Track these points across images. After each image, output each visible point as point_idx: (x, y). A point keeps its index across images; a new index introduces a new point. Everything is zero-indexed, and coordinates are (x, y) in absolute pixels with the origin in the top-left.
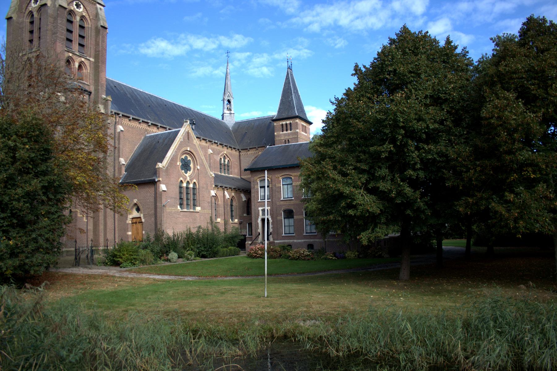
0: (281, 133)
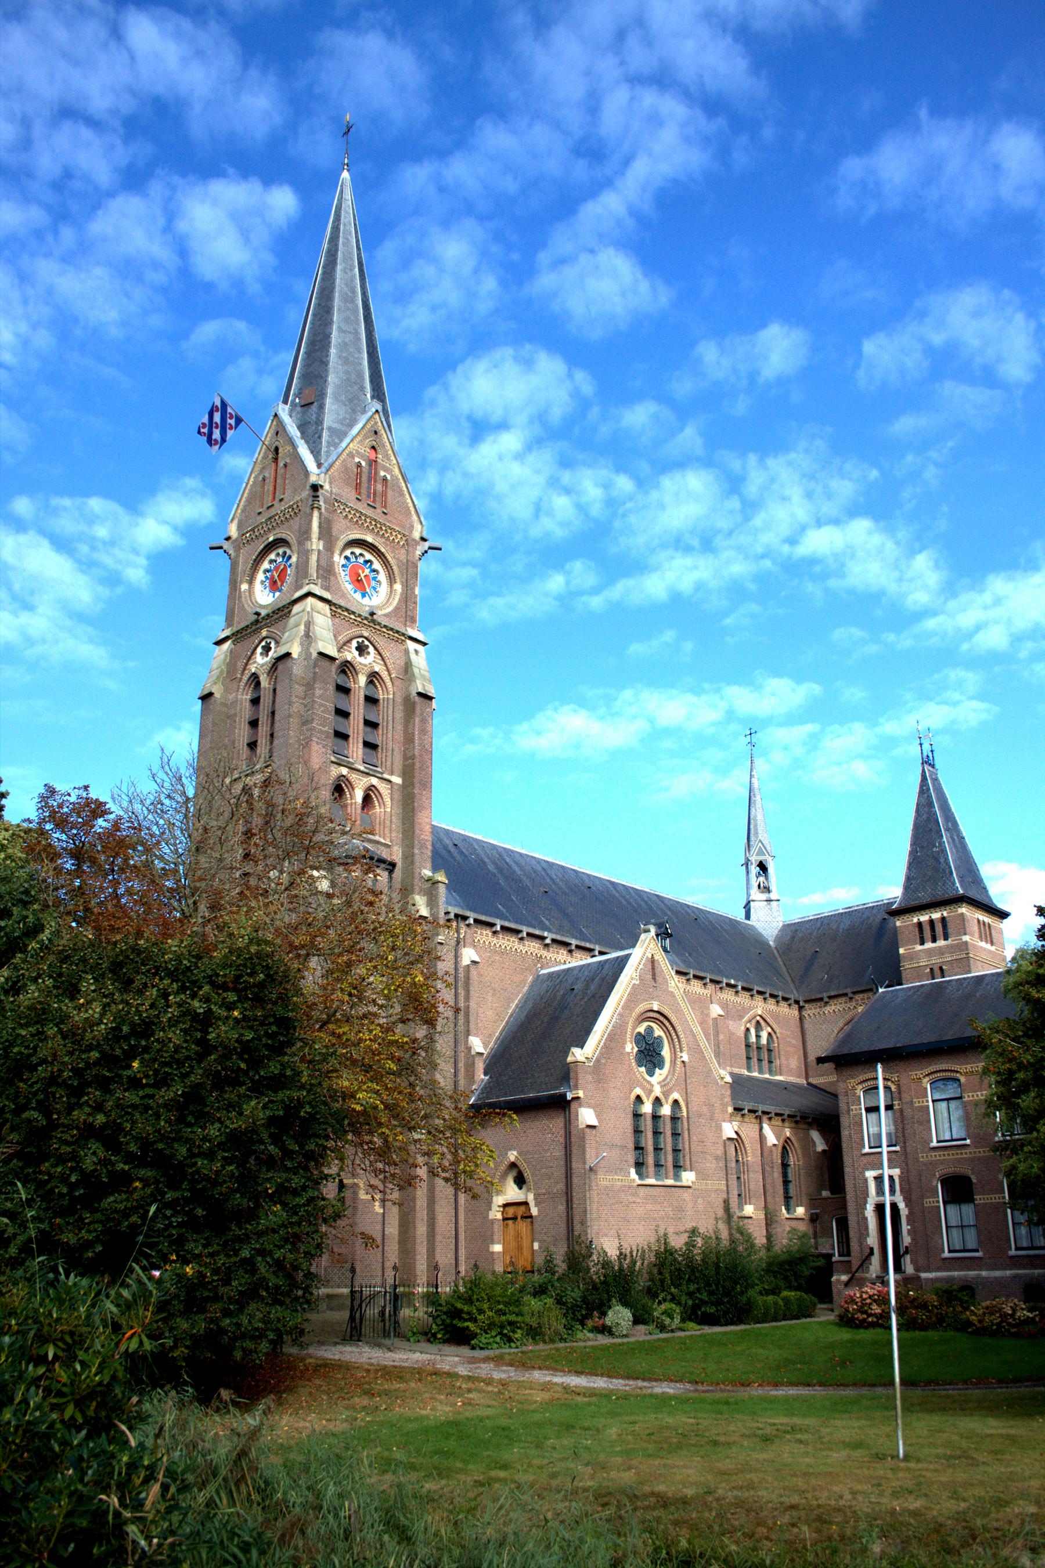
0: (919, 947)
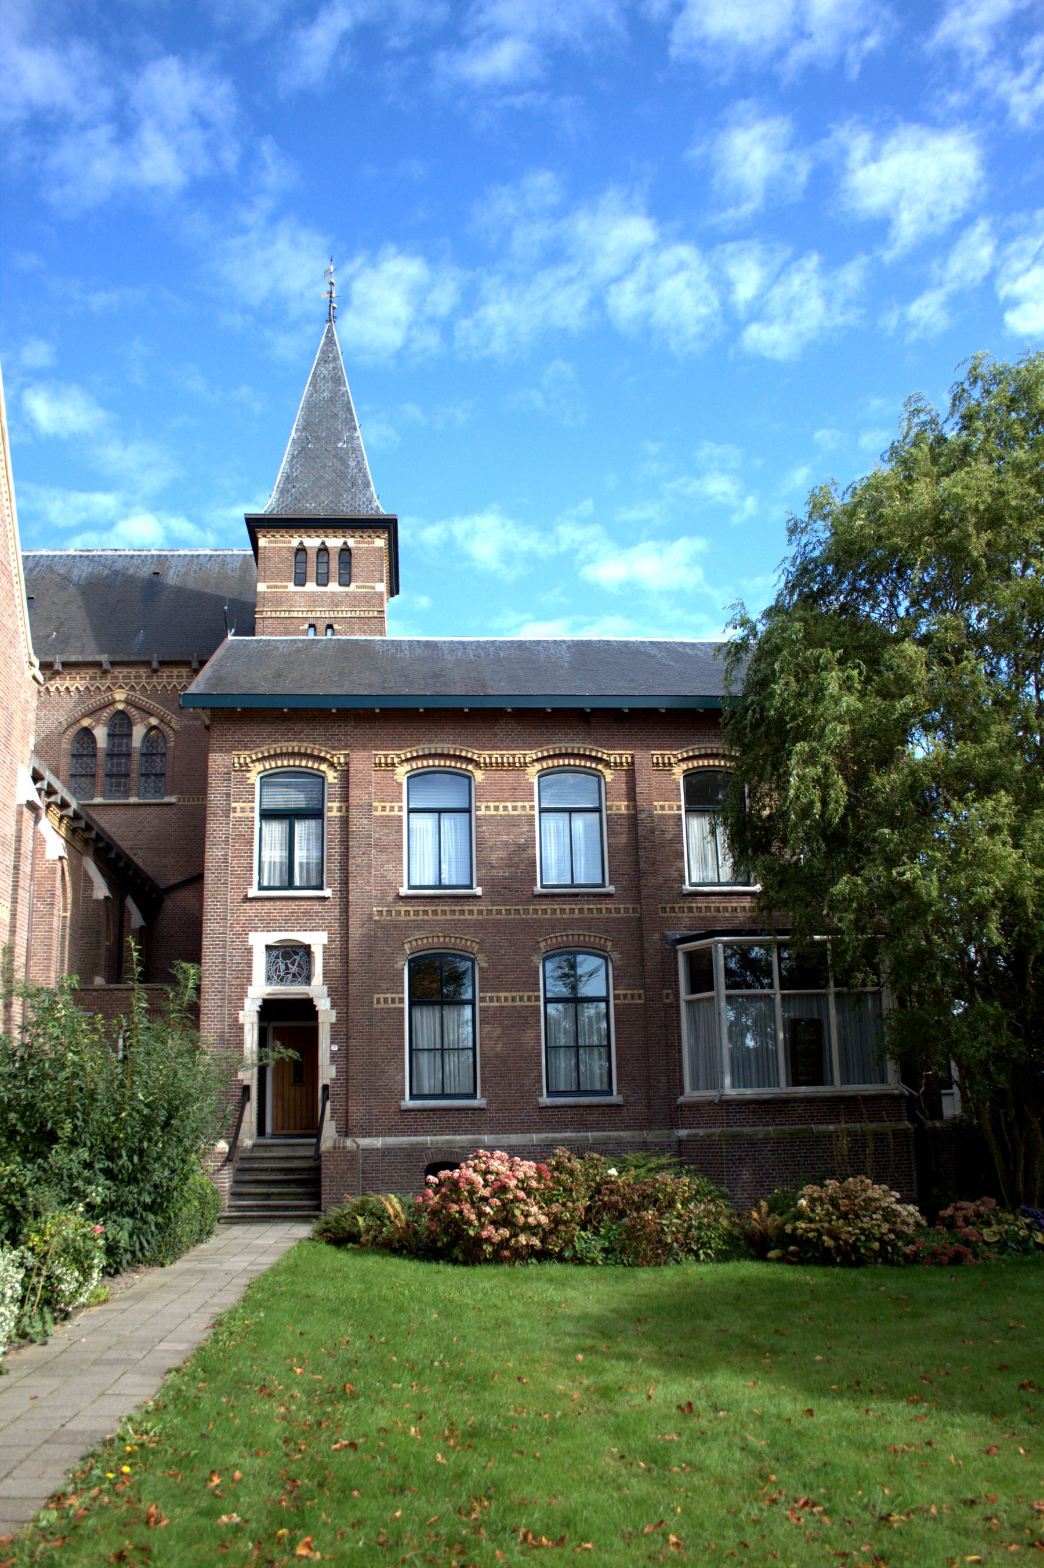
0: (291, 587)
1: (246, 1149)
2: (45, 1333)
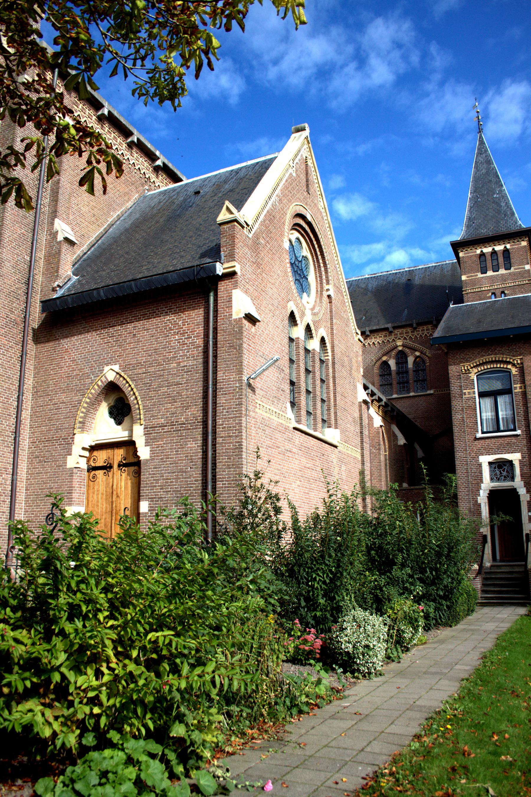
0: (480, 275)
1: (487, 568)
2: (399, 657)
